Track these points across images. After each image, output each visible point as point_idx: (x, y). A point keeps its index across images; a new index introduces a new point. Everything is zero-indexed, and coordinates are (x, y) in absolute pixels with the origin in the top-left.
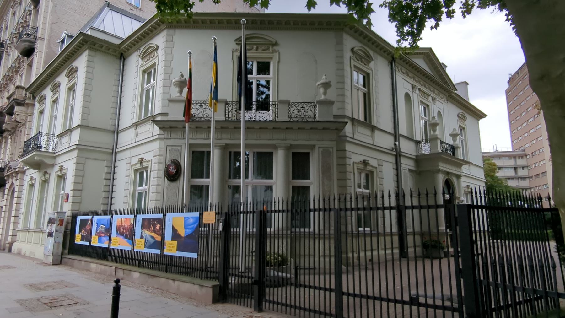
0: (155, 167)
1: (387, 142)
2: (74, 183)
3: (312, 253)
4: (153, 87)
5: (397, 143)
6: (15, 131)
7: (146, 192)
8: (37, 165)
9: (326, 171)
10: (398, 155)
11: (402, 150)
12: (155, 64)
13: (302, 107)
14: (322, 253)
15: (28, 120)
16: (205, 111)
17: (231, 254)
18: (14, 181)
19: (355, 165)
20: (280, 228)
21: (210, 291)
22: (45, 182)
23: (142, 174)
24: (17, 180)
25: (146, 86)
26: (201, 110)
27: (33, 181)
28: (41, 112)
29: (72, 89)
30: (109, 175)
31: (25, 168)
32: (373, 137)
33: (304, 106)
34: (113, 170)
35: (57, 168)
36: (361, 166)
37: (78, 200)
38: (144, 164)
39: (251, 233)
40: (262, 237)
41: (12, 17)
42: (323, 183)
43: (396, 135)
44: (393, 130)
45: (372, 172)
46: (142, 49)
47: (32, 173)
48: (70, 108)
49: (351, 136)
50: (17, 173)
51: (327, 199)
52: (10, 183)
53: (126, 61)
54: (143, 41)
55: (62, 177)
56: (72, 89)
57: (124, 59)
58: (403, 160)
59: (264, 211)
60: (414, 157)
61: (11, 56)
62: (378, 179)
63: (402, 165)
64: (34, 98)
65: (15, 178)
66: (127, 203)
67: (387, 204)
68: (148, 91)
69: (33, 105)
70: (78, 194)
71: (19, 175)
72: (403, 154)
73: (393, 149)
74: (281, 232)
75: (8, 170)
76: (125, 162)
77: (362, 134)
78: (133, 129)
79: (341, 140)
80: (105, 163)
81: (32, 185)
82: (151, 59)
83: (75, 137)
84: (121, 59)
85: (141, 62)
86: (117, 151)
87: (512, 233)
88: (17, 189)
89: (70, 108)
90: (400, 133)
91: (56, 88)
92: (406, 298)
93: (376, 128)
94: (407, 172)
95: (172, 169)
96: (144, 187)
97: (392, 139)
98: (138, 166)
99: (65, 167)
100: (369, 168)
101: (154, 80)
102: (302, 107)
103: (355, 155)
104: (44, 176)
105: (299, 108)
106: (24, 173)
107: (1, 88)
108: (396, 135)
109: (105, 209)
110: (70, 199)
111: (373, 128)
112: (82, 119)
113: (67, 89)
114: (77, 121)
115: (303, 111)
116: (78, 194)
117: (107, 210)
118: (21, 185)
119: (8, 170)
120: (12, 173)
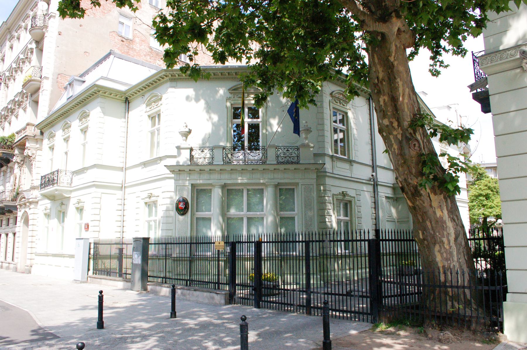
1: (366, 173)
5: (374, 174)
9: (307, 205)
10: (375, 184)
11: (379, 180)
19: (335, 197)
20: (269, 253)
21: (223, 297)
32: (351, 170)
33: (289, 149)
36: (340, 197)
37: (97, 229)
39: (291, 256)
40: (258, 259)
43: (374, 167)
44: (371, 162)
45: (350, 202)
49: (331, 171)
50: (31, 203)
51: (288, 235)
53: (130, 104)
57: (129, 103)
58: (380, 189)
60: (392, 185)
62: (356, 208)
63: (379, 193)
67: (314, 239)
72: (379, 183)
73: (370, 179)
74: (271, 255)
75: (20, 200)
77: (342, 169)
79: (321, 174)
84: (126, 103)
87: (287, 255)
90: (377, 164)
92: (345, 293)
93: (354, 161)
94: (384, 199)
95: (181, 205)
97: (370, 169)
99: (82, 200)
100: (347, 198)
103: (334, 187)
105: (285, 151)
107: (1, 119)
108: (374, 167)
111: (351, 162)
119: (20, 200)
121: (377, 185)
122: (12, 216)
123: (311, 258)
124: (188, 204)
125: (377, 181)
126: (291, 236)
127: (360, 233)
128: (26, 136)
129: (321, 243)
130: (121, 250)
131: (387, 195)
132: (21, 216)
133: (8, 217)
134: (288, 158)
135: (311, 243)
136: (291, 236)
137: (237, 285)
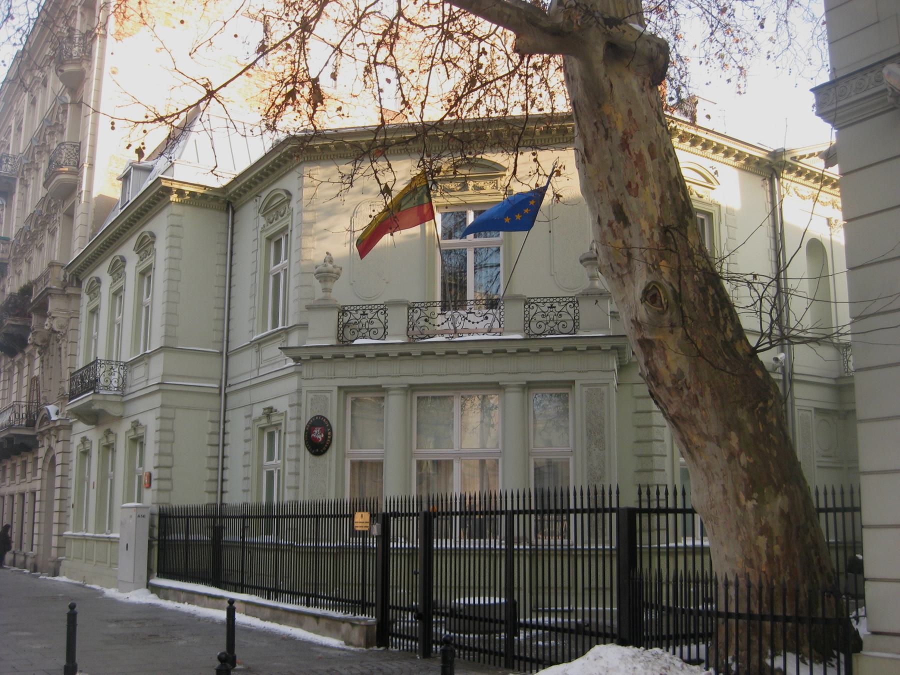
0: (292, 426)
2: (168, 291)
3: (608, 585)
4: (286, 270)
6: (48, 345)
7: (279, 471)
8: (93, 417)
12: (286, 227)
13: (552, 307)
14: (586, 585)
15: (70, 327)
16: (372, 323)
17: (435, 584)
18: (53, 445)
22: (109, 448)
23: (271, 436)
24: (58, 442)
25: (273, 268)
26: (364, 321)
27: (87, 446)
28: (94, 312)
29: (146, 274)
30: (215, 437)
31: (71, 421)
34: (222, 427)
35: (127, 425)
37: (165, 485)
38: (275, 419)
41: (29, 108)
42: (590, 454)
46: (264, 195)
47: (81, 428)
48: (143, 310)
50: (58, 429)
52: (46, 447)
54: (265, 181)
55: (138, 441)
56: (146, 274)
57: (234, 212)
59: (430, 513)
61: (30, 190)
63: (797, 402)
64: (79, 284)
65: (53, 439)
66: (248, 491)
68: (277, 277)
69: (79, 296)
70: (166, 473)
71: (62, 434)
76: (242, 413)
78: (254, 350)
80: (208, 415)
81: (86, 453)
82: (280, 218)
83: (157, 368)
84: (228, 213)
85: (262, 221)
86: (228, 390)
88: (59, 460)
89: (143, 310)
91: (117, 270)
96: (276, 461)
98: (264, 422)
101: (286, 259)
102: (552, 307)
104: (107, 437)
105: (545, 309)
106: (70, 427)
109: (214, 501)
110: (154, 484)
112: (166, 336)
113: (138, 275)
114: (156, 342)
115: (552, 315)
116: (166, 473)
117: (216, 504)
118: (66, 452)
120: (49, 430)
121: (791, 381)
122: (30, 458)
123: (516, 552)
124: (330, 427)
125: (792, 373)
126: (830, 496)
127: (649, 493)
128: (47, 289)
129: (848, 515)
130: (218, 532)
131: (818, 405)
132: (44, 456)
133: (24, 459)
134: (552, 324)
135: (516, 516)
136: (830, 496)
137: (390, 607)
